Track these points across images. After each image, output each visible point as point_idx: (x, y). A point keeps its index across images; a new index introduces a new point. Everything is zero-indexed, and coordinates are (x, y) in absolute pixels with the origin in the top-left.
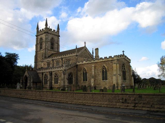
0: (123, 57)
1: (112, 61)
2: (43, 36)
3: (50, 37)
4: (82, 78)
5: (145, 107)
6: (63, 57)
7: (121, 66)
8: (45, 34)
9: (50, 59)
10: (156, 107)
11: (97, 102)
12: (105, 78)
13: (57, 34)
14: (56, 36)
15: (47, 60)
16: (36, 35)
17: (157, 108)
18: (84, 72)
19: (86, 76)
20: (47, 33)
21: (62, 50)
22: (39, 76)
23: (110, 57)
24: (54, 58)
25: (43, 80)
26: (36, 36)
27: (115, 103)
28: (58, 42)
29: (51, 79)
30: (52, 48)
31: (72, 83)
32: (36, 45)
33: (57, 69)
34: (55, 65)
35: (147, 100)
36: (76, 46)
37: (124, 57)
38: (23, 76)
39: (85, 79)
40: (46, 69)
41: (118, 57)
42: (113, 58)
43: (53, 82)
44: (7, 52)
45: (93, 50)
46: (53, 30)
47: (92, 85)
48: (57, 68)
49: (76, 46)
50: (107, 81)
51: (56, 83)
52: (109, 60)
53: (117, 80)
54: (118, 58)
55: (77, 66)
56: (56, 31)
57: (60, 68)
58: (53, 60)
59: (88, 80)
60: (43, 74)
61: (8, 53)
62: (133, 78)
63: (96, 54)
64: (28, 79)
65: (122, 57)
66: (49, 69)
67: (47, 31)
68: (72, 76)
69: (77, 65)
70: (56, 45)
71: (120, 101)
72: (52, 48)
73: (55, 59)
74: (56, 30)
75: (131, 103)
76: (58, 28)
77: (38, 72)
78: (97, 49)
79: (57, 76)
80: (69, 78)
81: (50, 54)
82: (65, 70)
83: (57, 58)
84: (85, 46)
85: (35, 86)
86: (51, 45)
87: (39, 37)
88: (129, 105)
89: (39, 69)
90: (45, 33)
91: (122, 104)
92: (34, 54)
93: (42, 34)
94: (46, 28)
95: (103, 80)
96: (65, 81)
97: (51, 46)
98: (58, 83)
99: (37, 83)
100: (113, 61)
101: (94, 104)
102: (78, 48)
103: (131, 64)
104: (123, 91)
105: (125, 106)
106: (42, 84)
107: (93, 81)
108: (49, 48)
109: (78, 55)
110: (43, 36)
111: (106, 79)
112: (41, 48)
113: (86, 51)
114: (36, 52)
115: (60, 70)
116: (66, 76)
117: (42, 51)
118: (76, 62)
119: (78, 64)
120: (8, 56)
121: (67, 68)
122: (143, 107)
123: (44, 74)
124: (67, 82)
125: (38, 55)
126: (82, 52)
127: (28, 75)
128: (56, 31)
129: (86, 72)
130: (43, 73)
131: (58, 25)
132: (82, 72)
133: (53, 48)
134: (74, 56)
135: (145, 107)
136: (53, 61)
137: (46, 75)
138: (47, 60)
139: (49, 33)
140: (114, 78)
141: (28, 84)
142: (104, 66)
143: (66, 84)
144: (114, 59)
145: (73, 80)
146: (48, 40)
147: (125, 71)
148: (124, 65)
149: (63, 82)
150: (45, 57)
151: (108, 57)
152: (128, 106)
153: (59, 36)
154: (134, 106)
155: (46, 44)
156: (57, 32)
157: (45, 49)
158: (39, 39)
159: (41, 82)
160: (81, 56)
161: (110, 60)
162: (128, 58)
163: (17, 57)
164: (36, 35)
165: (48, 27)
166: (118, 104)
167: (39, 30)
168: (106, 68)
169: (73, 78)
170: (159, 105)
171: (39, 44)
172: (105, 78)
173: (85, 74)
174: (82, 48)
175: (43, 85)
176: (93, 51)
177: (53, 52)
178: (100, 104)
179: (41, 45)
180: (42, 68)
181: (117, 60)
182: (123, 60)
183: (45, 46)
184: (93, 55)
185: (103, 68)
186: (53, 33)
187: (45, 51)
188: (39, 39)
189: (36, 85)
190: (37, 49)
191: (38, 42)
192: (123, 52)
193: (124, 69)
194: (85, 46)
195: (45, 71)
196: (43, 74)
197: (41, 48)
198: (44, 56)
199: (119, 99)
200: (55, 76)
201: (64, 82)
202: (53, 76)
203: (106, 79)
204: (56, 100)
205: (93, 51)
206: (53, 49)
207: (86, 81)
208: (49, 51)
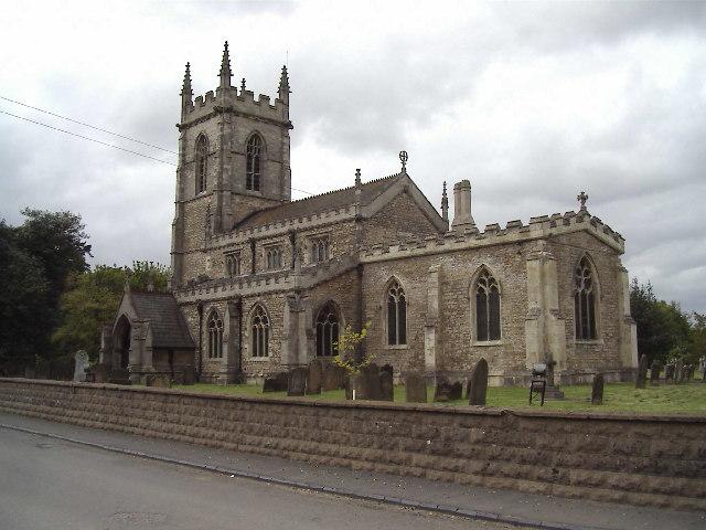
0: (581, 226)
1: (520, 243)
2: (212, 129)
3: (244, 130)
4: (385, 326)
5: (527, 474)
6: (296, 225)
7: (568, 268)
8: (218, 119)
9: (241, 237)
10: (575, 478)
11: (334, 448)
13: (276, 116)
16: (178, 125)
17: (579, 483)
18: (481, 290)
20: (230, 110)
21: (297, 195)
22: (184, 319)
23: (515, 225)
24: (256, 234)
25: (204, 336)
26: (182, 128)
27: (403, 455)
28: (282, 153)
29: (237, 333)
30: (254, 182)
32: (181, 172)
34: (262, 263)
35: (540, 441)
36: (358, 175)
37: (586, 224)
39: (398, 333)
40: (222, 283)
41: (553, 225)
43: (247, 346)
44: (31, 209)
45: (445, 190)
46: (256, 99)
47: (430, 360)
48: (273, 281)
49: (358, 175)
50: (498, 342)
51: (261, 355)
53: (545, 341)
54: (554, 231)
56: (272, 103)
57: (241, 284)
58: (253, 242)
59: (410, 336)
60: (201, 310)
61: (35, 214)
62: (634, 329)
63: (458, 211)
64: (133, 332)
65: (574, 225)
66: (237, 286)
67: (230, 103)
68: (334, 319)
69: (361, 266)
70: (270, 171)
71: (425, 446)
72: (254, 182)
73: (261, 235)
74: (274, 96)
75: (469, 458)
76: (284, 87)
77: (183, 298)
79: (265, 321)
80: (319, 329)
81: (245, 213)
82: (298, 291)
83: (272, 231)
84: (404, 169)
85: (166, 364)
86: (249, 168)
87: (194, 132)
88: (462, 462)
89: (192, 284)
90: (218, 111)
91: (432, 459)
93: (208, 118)
94: (226, 87)
95: (481, 337)
97: (249, 176)
101: (324, 454)
102: (364, 180)
104: (534, 394)
105: (445, 469)
106: (197, 356)
107: (432, 344)
108: (240, 186)
109: (364, 215)
110: (212, 129)
111: (496, 335)
112: (201, 185)
113: (411, 196)
114: (181, 204)
115: (279, 286)
116: (306, 320)
119: (364, 258)
120: (33, 224)
121: (308, 281)
122: (518, 476)
124: (310, 349)
125: (189, 220)
126: (390, 205)
127: (132, 315)
128: (272, 103)
130: (200, 306)
131: (285, 73)
133: (257, 182)
134: (350, 221)
135: (527, 476)
136: (253, 248)
137: (214, 313)
139: (237, 114)
140: (532, 332)
141: (132, 359)
143: (305, 357)
144: (534, 234)
146: (234, 138)
147: (592, 297)
148: (584, 262)
149: (290, 346)
150: (220, 229)
151: (503, 227)
152: (456, 470)
153: (289, 126)
154: (484, 473)
155: (222, 164)
156: (280, 106)
157: (220, 189)
160: (382, 219)
162: (608, 230)
163: (76, 231)
164: (178, 125)
165: (235, 82)
166: (416, 458)
167: (193, 99)
168: (401, 290)
170: (587, 469)
171: (194, 164)
172: (488, 327)
173: (397, 308)
175: (200, 364)
176: (445, 194)
177: (257, 204)
178: (345, 457)
179: (201, 170)
180: (204, 279)
182: (583, 240)
183: (220, 174)
184: (445, 214)
185: (483, 282)
186: (257, 111)
188: (192, 143)
189: (170, 361)
190: (181, 190)
192: (583, 198)
193: (588, 283)
194: (404, 169)
195: (211, 295)
196: (201, 310)
197: (201, 185)
198: (213, 224)
199: (369, 432)
202: (248, 320)
203: (496, 335)
204: (177, 433)
205: (445, 194)
206: (257, 188)
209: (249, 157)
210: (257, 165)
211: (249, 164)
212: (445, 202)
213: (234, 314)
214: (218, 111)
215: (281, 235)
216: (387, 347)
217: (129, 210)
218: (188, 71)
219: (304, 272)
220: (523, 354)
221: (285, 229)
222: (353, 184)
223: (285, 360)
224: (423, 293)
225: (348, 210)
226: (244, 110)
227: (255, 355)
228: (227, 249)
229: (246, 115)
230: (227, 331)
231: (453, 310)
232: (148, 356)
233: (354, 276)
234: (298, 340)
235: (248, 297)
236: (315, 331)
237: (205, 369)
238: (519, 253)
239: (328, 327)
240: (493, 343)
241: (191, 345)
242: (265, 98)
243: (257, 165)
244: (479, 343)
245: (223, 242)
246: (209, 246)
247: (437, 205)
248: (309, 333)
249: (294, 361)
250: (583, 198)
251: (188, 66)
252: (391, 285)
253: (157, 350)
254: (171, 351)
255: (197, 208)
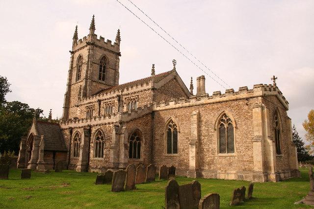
1: (247, 99)
3: (99, 54)
7: (272, 111)
9: (95, 99)
12: (226, 146)
14: (113, 52)
15: (88, 101)
16: (70, 51)
18: (170, 129)
19: (132, 145)
22: (63, 137)
25: (72, 145)
26: (72, 53)
28: (116, 66)
30: (102, 77)
31: (139, 157)
33: (103, 121)
34: (103, 112)
37: (275, 93)
38: (26, 135)
39: (173, 147)
42: (251, 91)
45: (192, 81)
46: (98, 38)
51: (99, 157)
52: (238, 96)
55: (153, 113)
58: (100, 101)
60: (71, 132)
65: (273, 93)
68: (138, 139)
70: (110, 73)
72: (102, 77)
76: (118, 38)
78: (202, 78)
80: (131, 143)
82: (121, 123)
86: (100, 71)
87: (77, 55)
90: (88, 44)
92: (65, 90)
96: (119, 152)
97: (100, 74)
98: (102, 157)
99: (57, 153)
100: (251, 101)
102: (157, 73)
103: (289, 113)
108: (96, 78)
109: (156, 87)
111: (231, 150)
112: (78, 77)
117: (81, 84)
118: (152, 105)
119: (156, 108)
121: (126, 118)
123: (74, 132)
124: (125, 155)
125: (72, 93)
126: (169, 85)
128: (113, 44)
129: (175, 129)
130: (71, 130)
132: (165, 132)
137: (77, 134)
138: (88, 101)
139: (97, 46)
142: (225, 114)
143: (123, 158)
144: (256, 94)
145: (142, 150)
146: (98, 62)
150: (85, 96)
153: (119, 54)
155: (88, 67)
158: (75, 59)
159: (66, 152)
161: (239, 98)
162: (284, 98)
169: (143, 145)
172: (226, 146)
173: (172, 136)
174: (168, 74)
175: (69, 159)
177: (103, 87)
179: (79, 71)
180: (76, 118)
181: (262, 96)
183: (87, 71)
184: (192, 91)
187: (86, 82)
188: (75, 59)
191: (74, 65)
192: (274, 79)
196: (71, 132)
197: (78, 77)
198: (82, 94)
200: (98, 138)
201: (118, 155)
202: (93, 138)
203: (231, 150)
207: (174, 153)
208: (94, 84)
209: (101, 66)
210: (104, 70)
211: (101, 69)
212: (192, 86)
213: (87, 135)
214: (88, 44)
215: (113, 98)
216: (167, 155)
217: (43, 90)
218: (76, 29)
219: (124, 113)
220: (251, 162)
221: (115, 95)
222: (150, 75)
223: (112, 161)
224: (187, 130)
225: (147, 84)
226: (100, 45)
227: (96, 157)
228: (87, 105)
229: (101, 47)
230: (83, 143)
231: (206, 136)
232: (41, 155)
233: (149, 118)
234: (119, 150)
235: (94, 126)
236: (129, 145)
237: (72, 162)
238: (247, 104)
239: (135, 143)
240: (230, 154)
241: (65, 150)
242: (109, 41)
243: (104, 70)
244: (220, 155)
245: (86, 102)
246: (79, 104)
247: (189, 87)
248: (125, 145)
249: (117, 161)
250: (274, 79)
251: (77, 27)
252: (97, 134)
253: (46, 152)
254: (54, 152)
255: (75, 88)
